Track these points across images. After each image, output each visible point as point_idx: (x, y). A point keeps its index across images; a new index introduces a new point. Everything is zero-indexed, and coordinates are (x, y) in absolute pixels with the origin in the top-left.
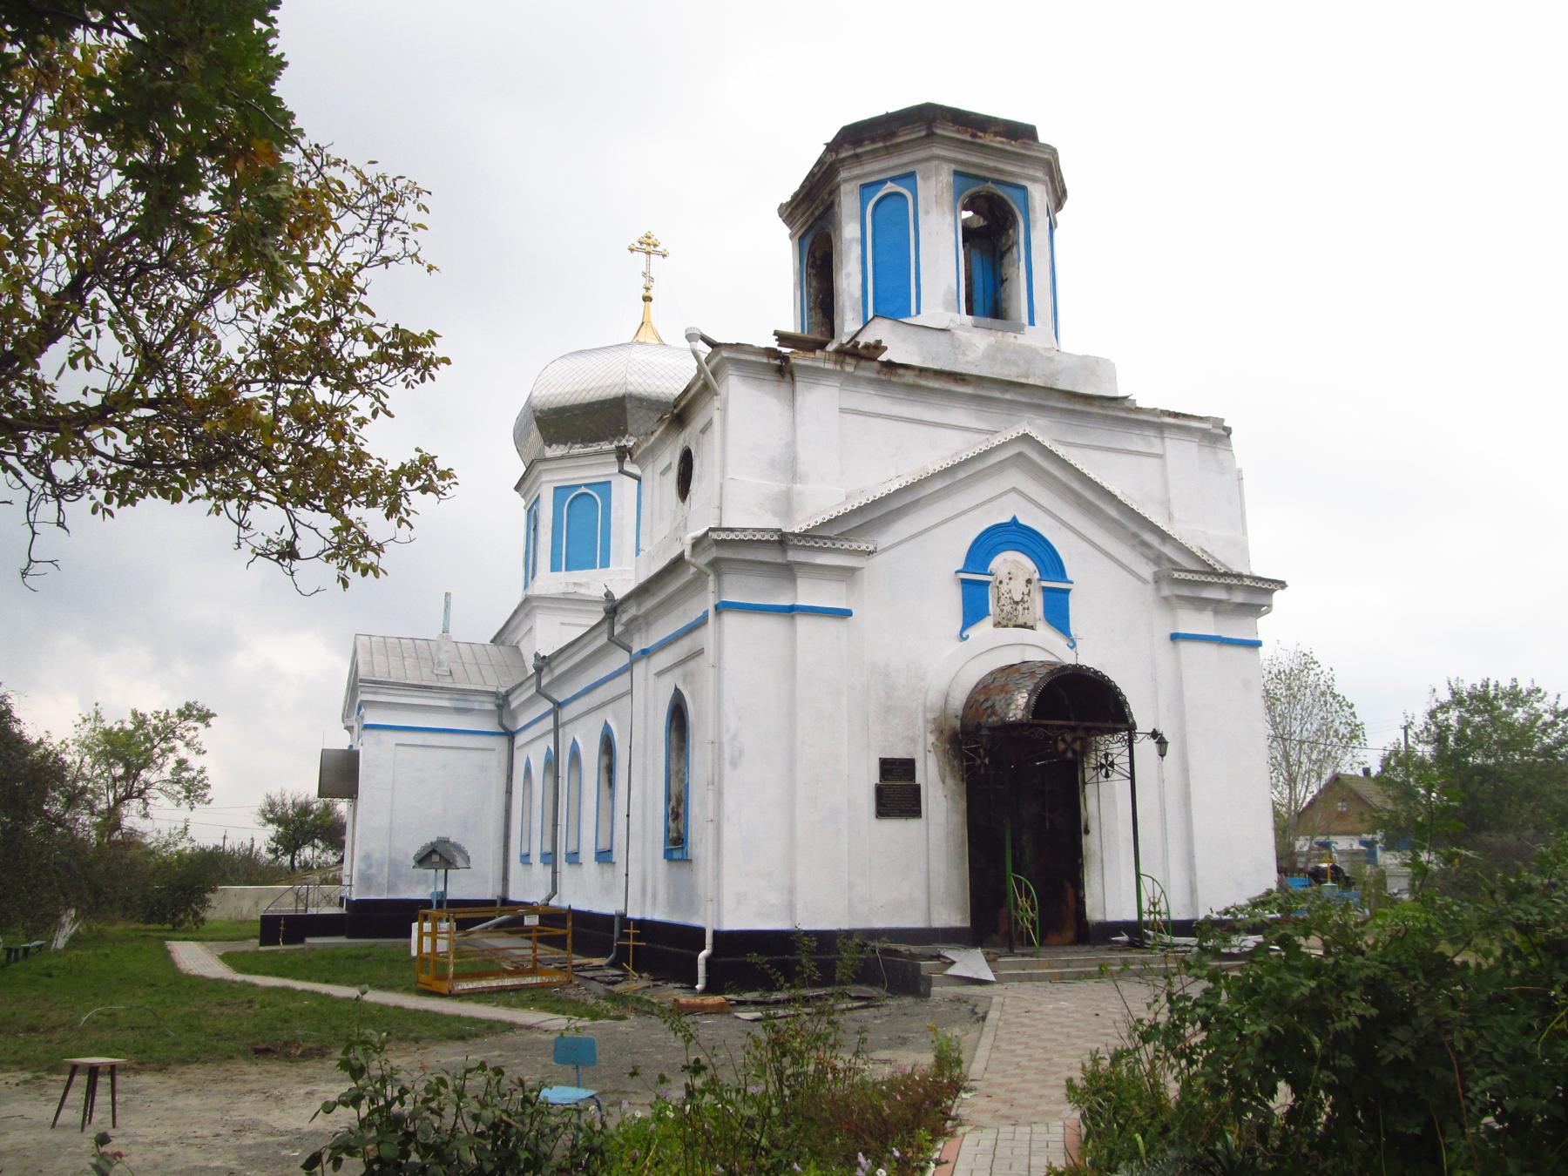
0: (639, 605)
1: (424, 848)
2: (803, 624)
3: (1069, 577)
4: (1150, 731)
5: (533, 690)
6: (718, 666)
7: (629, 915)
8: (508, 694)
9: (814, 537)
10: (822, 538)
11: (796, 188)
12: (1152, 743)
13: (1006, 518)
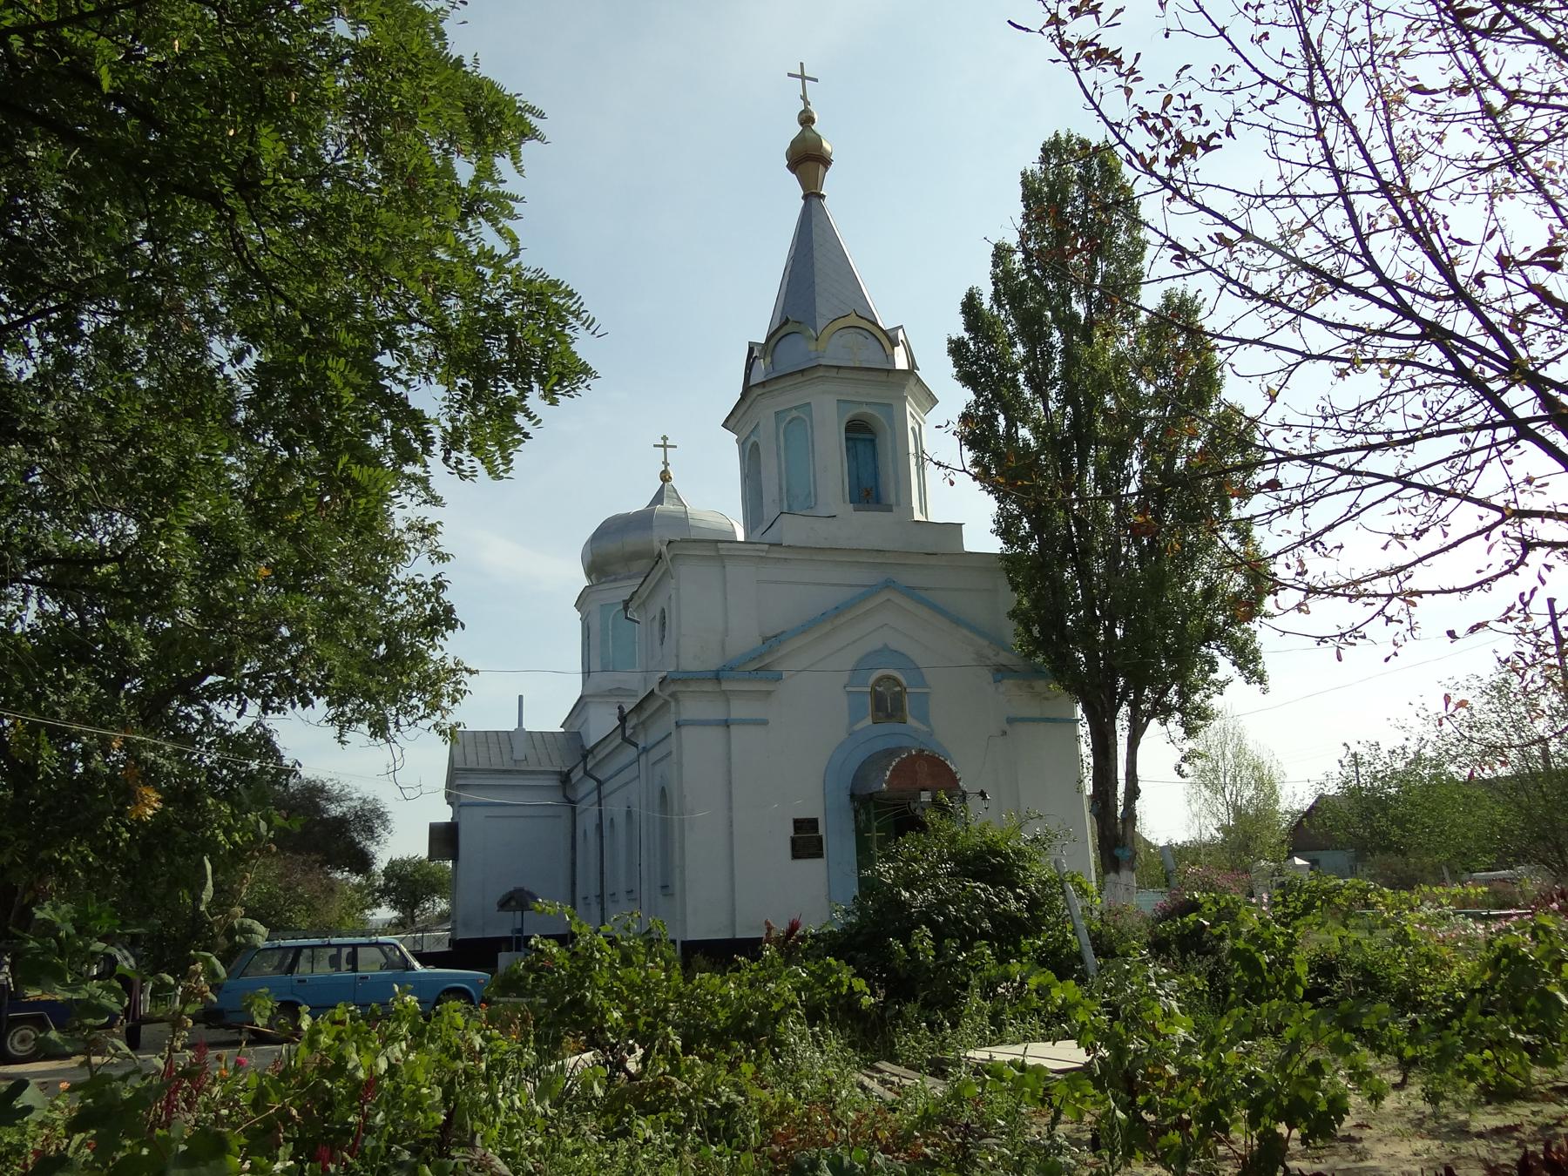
0: (638, 717)
5: (582, 774)
6: (680, 764)
8: (570, 772)
9: (1362, 448)
10: (1357, 449)
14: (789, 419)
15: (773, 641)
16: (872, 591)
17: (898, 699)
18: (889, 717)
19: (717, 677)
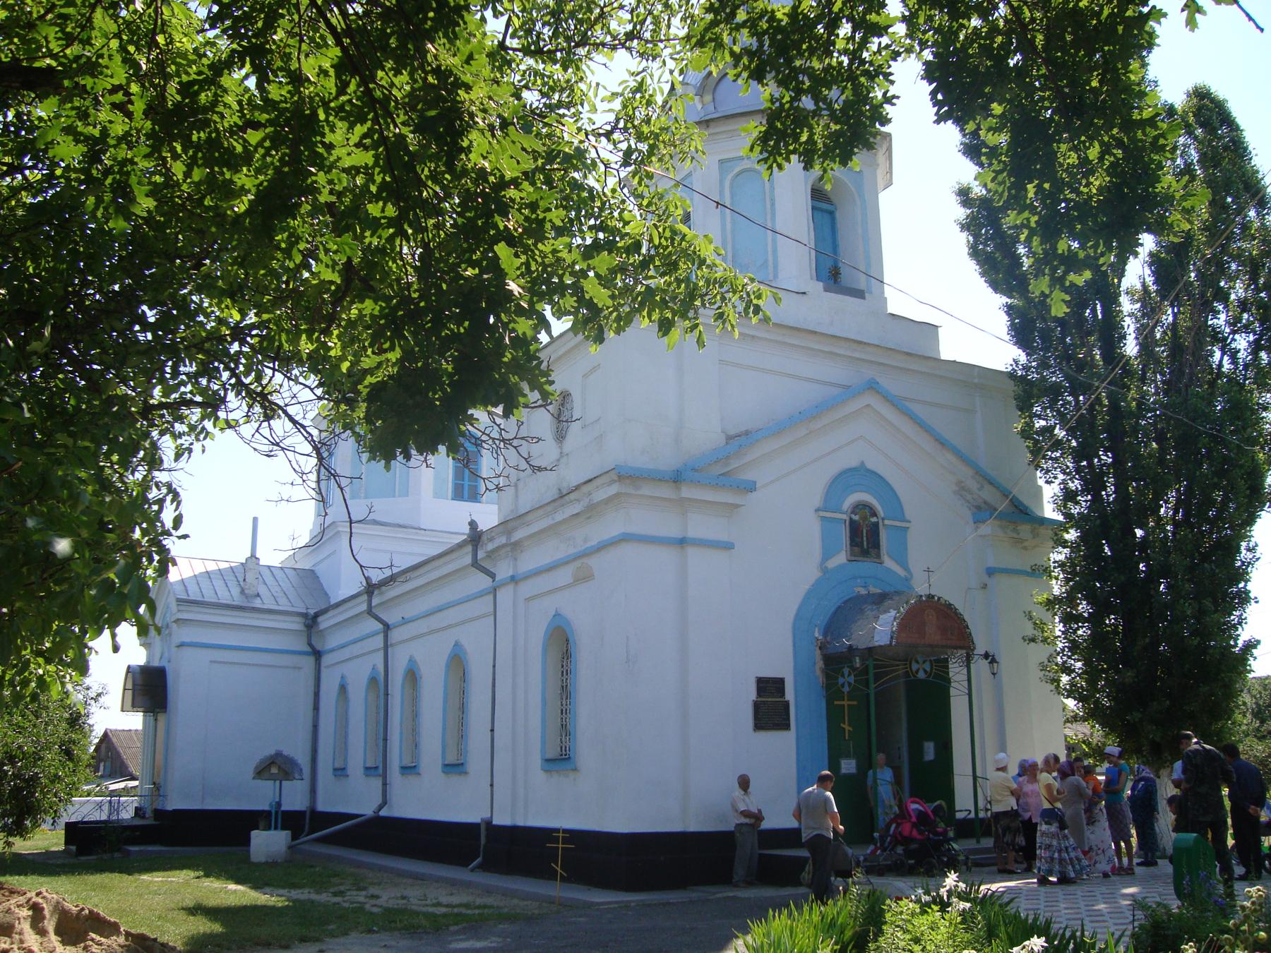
1: (262, 762)
2: (691, 551)
3: (908, 516)
4: (983, 653)
7: (495, 822)
8: (317, 615)
11: (1234, 114)
12: (985, 663)
13: (854, 463)
14: (737, 170)
15: (739, 440)
16: (848, 392)
17: (874, 530)
18: (865, 553)
19: (677, 478)
